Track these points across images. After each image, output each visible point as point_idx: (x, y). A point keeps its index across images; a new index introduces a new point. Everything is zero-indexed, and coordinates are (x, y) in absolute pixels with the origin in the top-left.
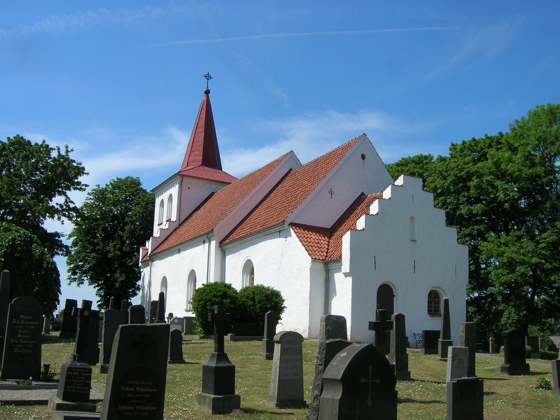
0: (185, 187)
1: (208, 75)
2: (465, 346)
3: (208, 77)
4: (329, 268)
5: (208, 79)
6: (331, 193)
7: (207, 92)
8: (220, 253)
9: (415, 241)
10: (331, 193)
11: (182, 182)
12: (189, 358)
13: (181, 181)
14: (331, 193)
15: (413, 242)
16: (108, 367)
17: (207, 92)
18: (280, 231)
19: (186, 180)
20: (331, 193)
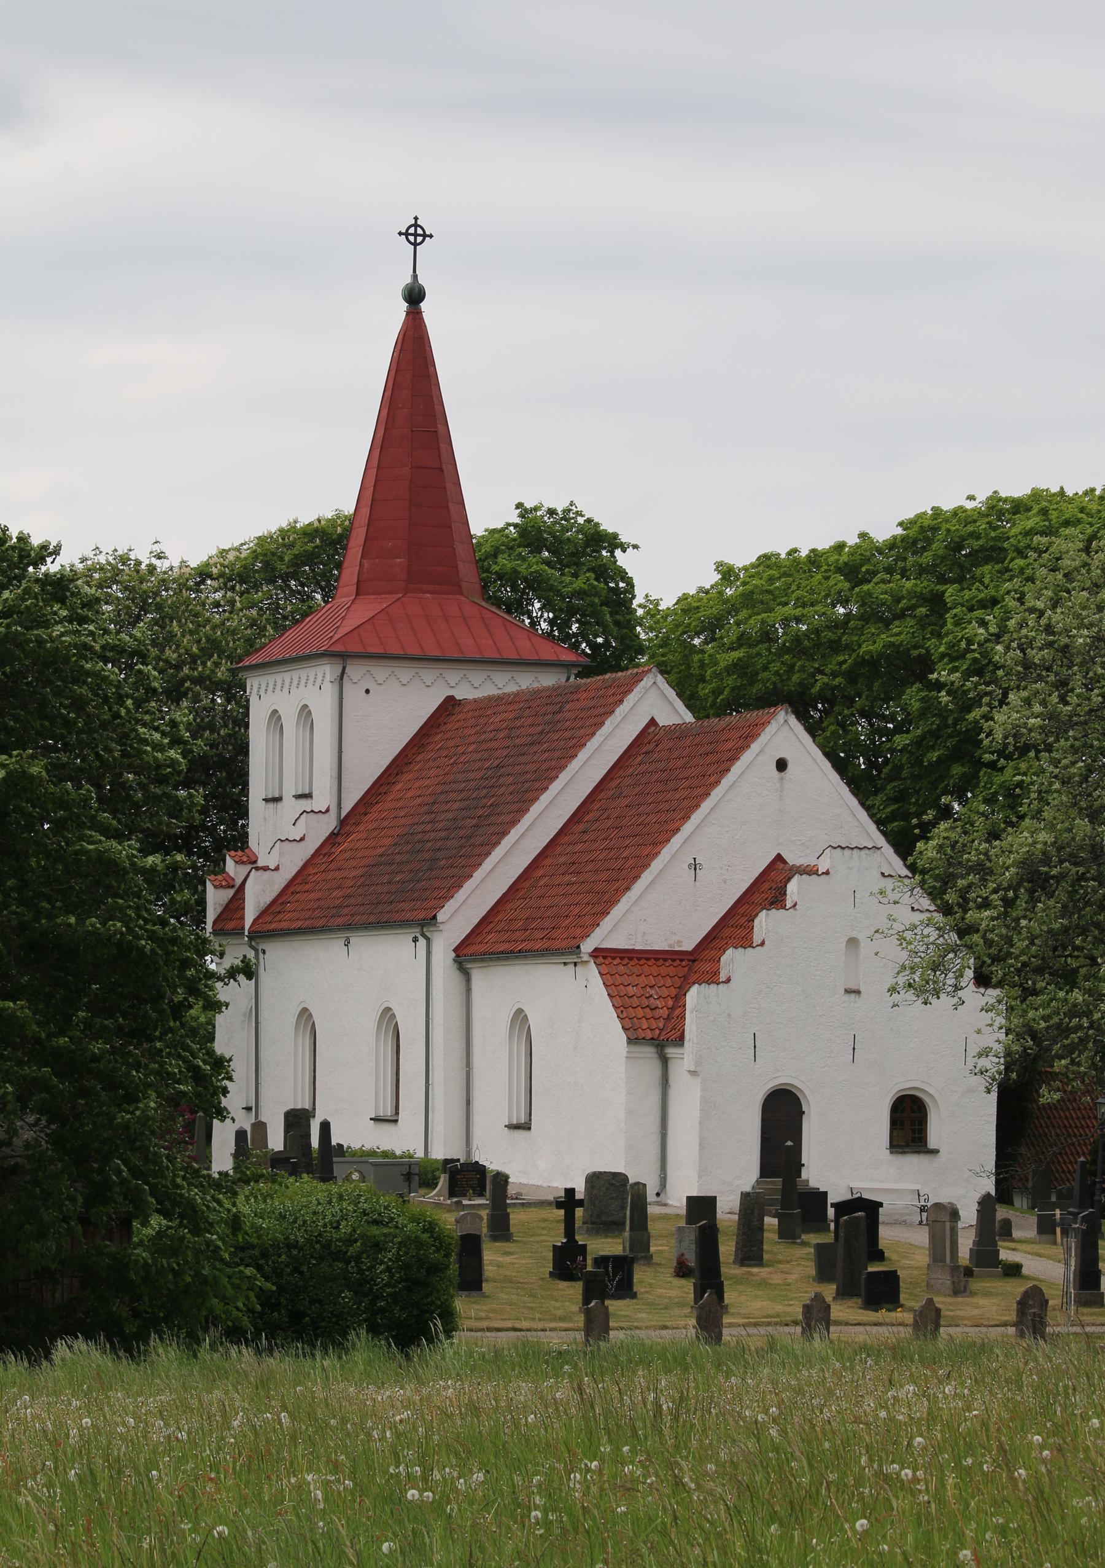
0: (353, 694)
1: (416, 225)
2: (624, 1230)
3: (415, 235)
4: (668, 1056)
5: (415, 244)
6: (695, 869)
7: (414, 296)
8: (456, 976)
9: (857, 992)
10: (695, 869)
11: (342, 678)
12: (648, 1364)
13: (340, 671)
14: (695, 866)
15: (853, 995)
16: (77, 1337)
17: (414, 296)
18: (575, 964)
19: (355, 671)
20: (695, 866)
